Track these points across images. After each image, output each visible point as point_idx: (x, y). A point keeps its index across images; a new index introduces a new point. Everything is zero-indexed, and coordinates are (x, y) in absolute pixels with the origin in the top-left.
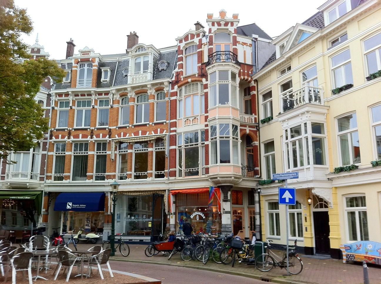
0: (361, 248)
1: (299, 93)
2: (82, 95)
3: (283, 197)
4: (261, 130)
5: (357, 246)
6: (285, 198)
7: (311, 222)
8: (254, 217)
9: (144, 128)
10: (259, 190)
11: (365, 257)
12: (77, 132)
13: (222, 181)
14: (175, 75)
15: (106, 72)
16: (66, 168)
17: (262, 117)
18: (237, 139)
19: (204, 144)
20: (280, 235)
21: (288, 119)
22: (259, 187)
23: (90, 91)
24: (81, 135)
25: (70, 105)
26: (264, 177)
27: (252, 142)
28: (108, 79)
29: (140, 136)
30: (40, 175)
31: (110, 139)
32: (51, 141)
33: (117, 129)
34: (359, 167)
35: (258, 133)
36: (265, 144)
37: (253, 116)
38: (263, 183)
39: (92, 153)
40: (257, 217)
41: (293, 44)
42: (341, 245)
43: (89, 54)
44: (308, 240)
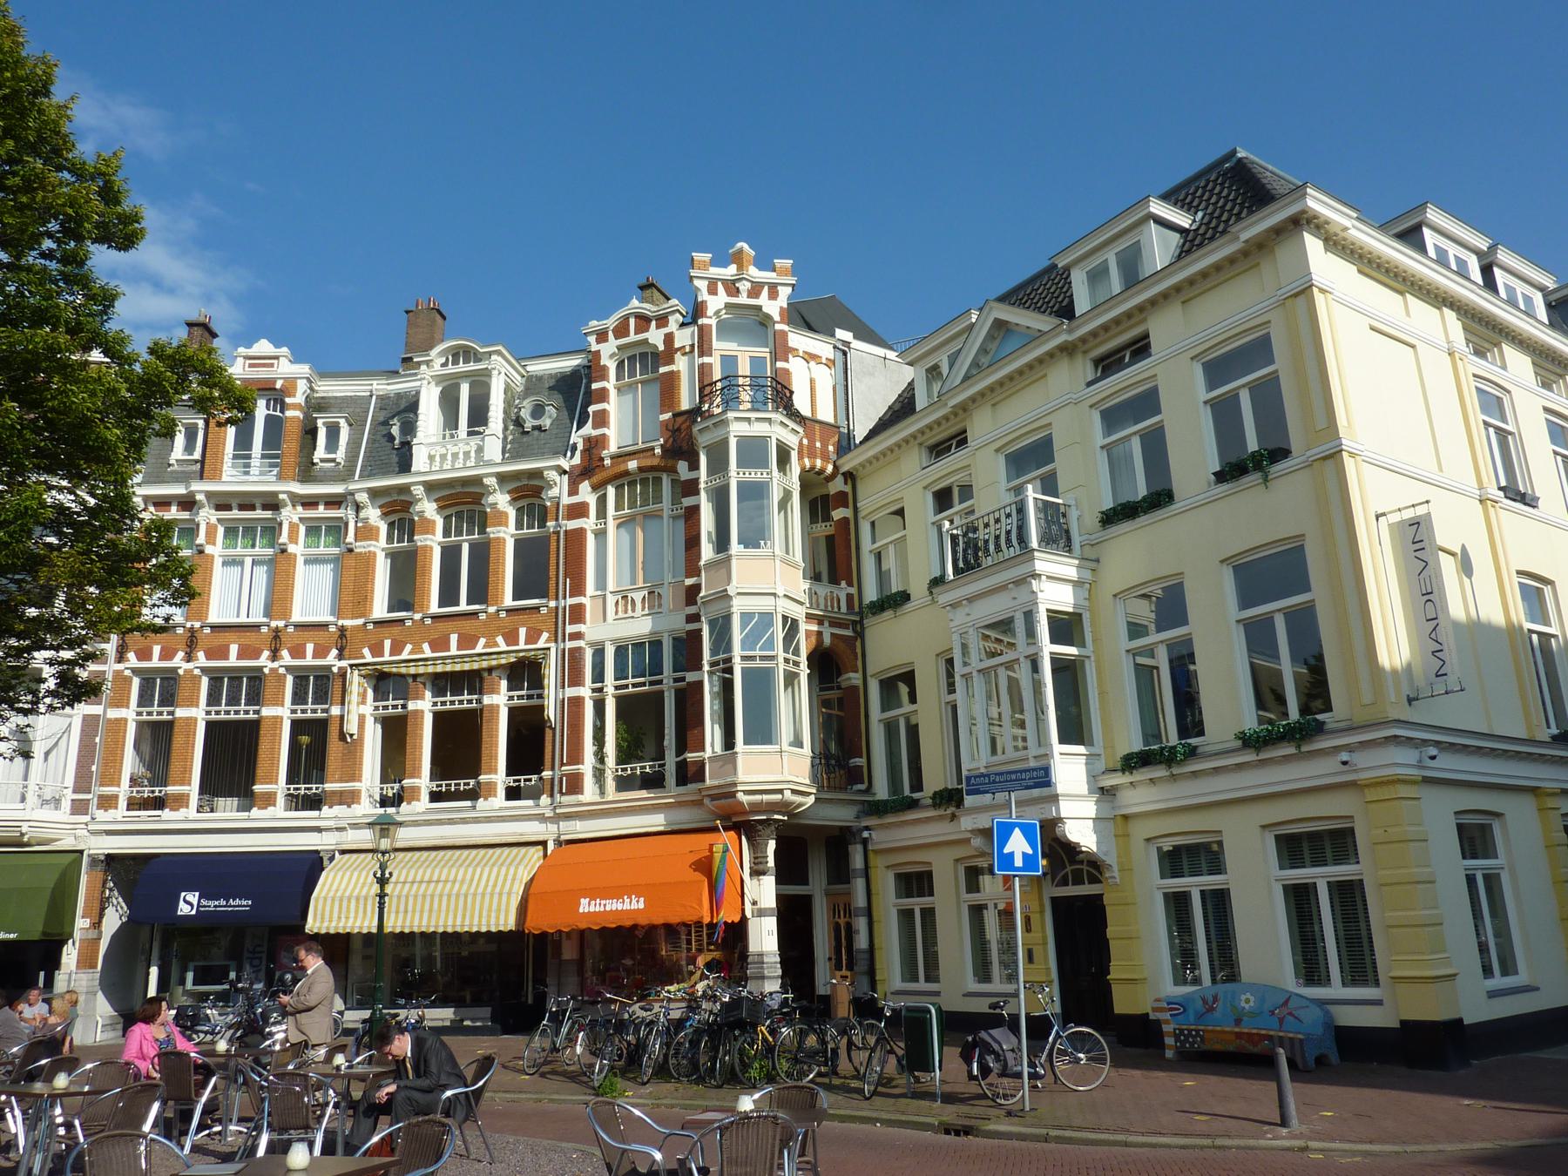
0: (1219, 1006)
1: (992, 522)
2: (242, 507)
3: (1006, 851)
4: (868, 634)
5: (1204, 1001)
6: (1012, 854)
7: (1044, 931)
8: (849, 926)
9: (467, 625)
10: (866, 834)
11: (1239, 1035)
12: (222, 638)
13: (751, 804)
14: (580, 447)
15: (333, 431)
16: (175, 766)
17: (871, 594)
18: (796, 664)
19: (683, 679)
20: (936, 980)
21: (971, 600)
22: (864, 824)
23: (275, 494)
24: (234, 649)
25: (198, 541)
26: (882, 791)
27: (839, 674)
28: (340, 455)
29: (454, 651)
30: (75, 792)
31: (344, 663)
32: (120, 667)
33: (370, 626)
34: (1200, 750)
35: (858, 644)
36: (881, 682)
37: (843, 590)
38: (878, 809)
39: (281, 712)
40: (861, 924)
41: (975, 364)
42: (1158, 1000)
43: (272, 365)
44: (1034, 987)
